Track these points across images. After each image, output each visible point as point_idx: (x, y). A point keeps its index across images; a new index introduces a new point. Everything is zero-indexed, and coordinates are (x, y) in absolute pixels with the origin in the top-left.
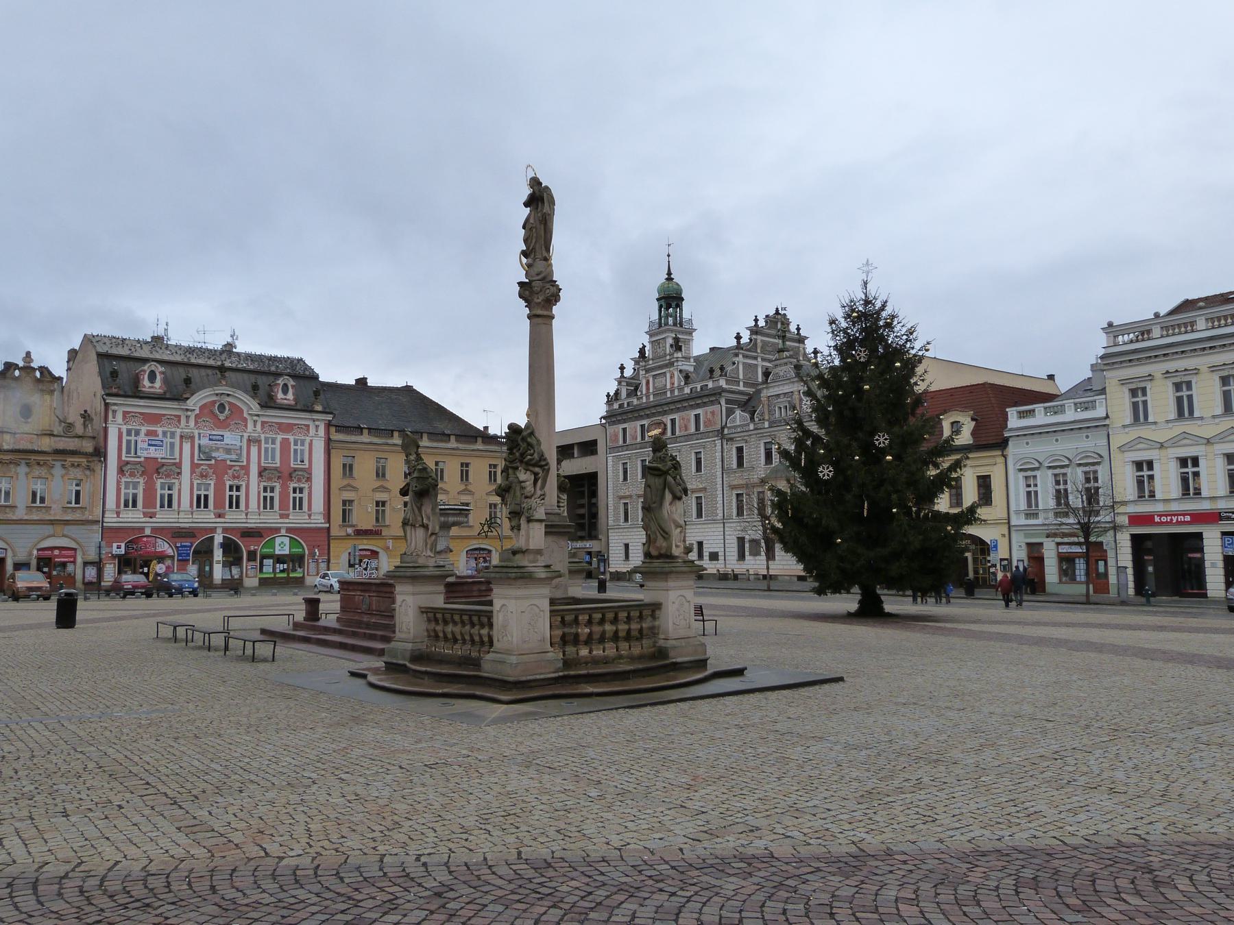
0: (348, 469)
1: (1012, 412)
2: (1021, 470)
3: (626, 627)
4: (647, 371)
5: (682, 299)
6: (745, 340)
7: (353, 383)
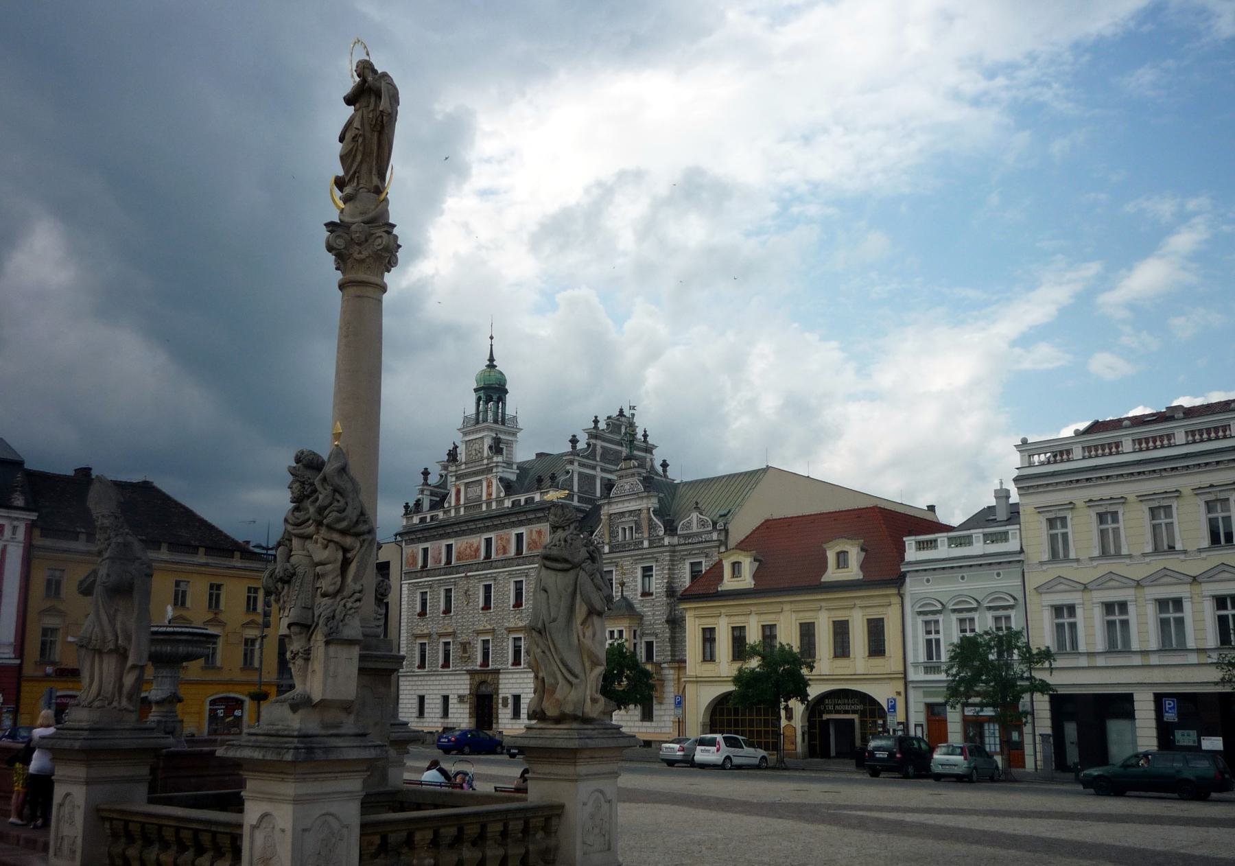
0: (53, 587)
1: (910, 542)
2: (920, 613)
3: (501, 852)
4: (458, 478)
5: (506, 392)
6: (581, 445)
7: (71, 473)
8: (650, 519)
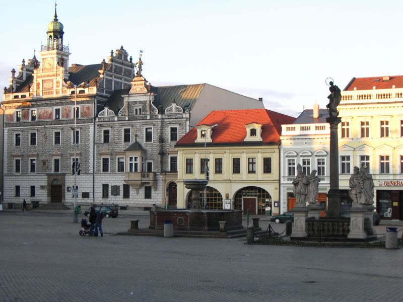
2: (287, 156)
8: (150, 106)
